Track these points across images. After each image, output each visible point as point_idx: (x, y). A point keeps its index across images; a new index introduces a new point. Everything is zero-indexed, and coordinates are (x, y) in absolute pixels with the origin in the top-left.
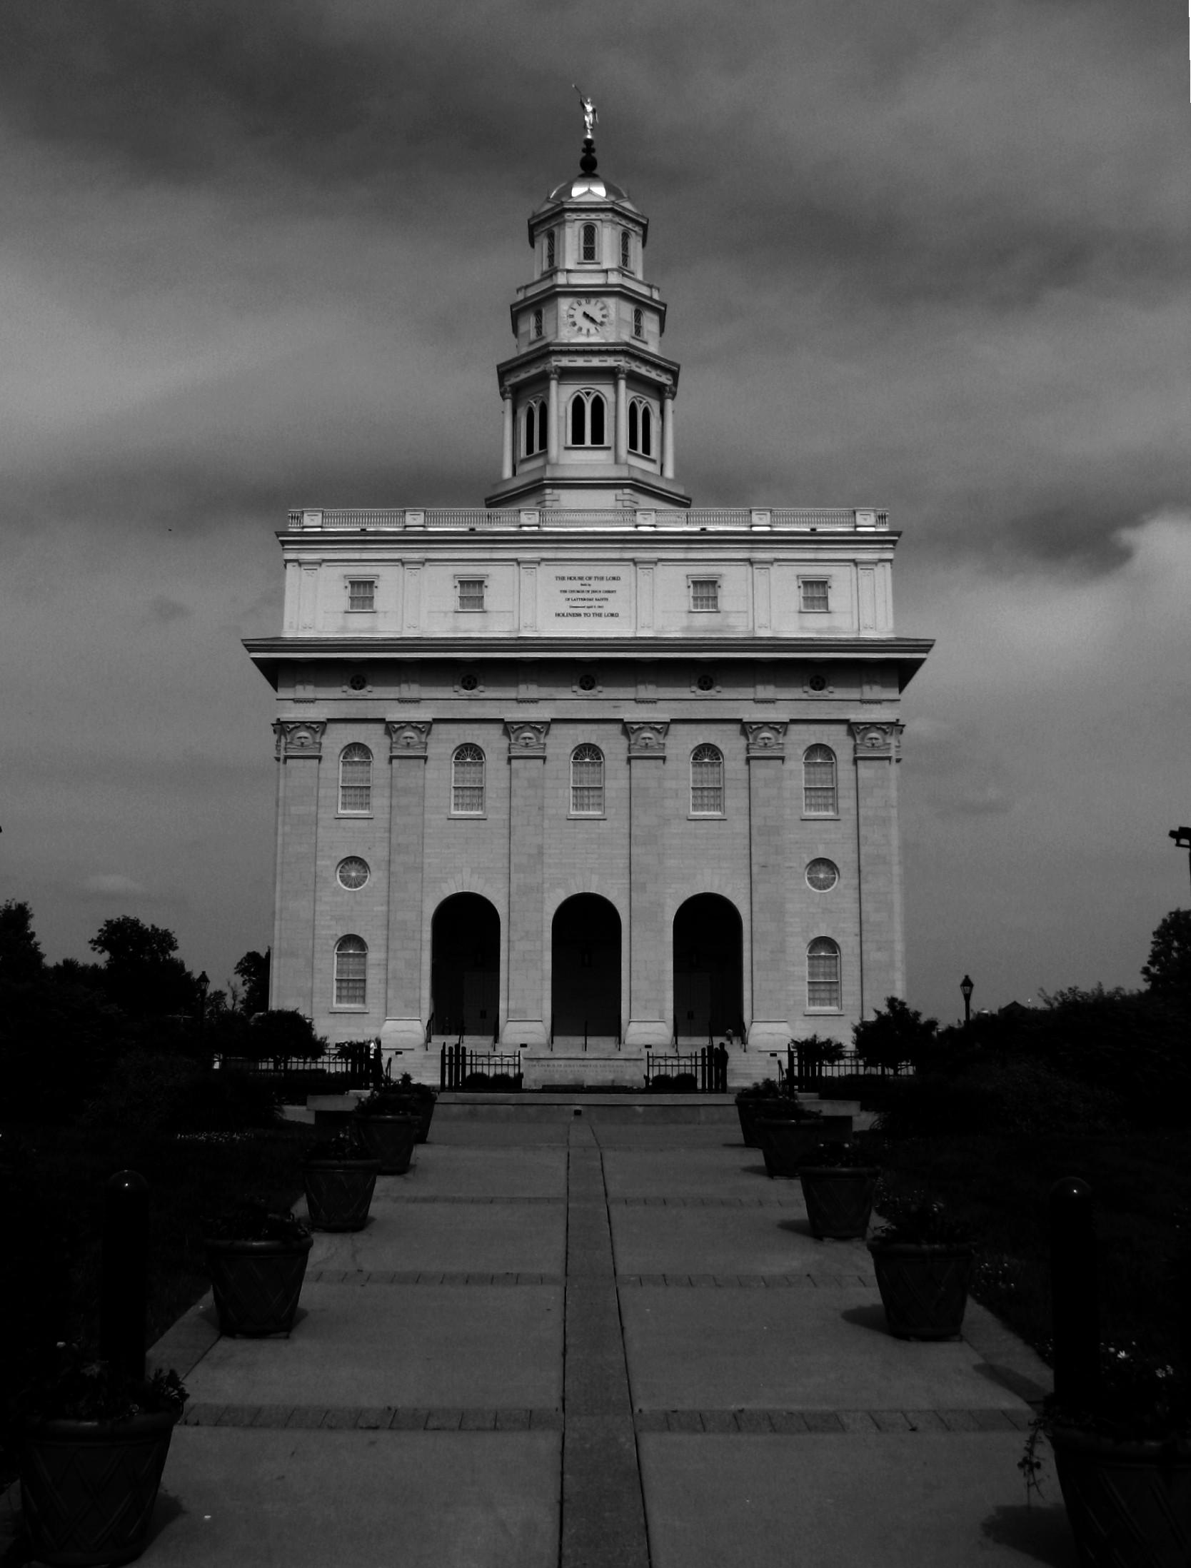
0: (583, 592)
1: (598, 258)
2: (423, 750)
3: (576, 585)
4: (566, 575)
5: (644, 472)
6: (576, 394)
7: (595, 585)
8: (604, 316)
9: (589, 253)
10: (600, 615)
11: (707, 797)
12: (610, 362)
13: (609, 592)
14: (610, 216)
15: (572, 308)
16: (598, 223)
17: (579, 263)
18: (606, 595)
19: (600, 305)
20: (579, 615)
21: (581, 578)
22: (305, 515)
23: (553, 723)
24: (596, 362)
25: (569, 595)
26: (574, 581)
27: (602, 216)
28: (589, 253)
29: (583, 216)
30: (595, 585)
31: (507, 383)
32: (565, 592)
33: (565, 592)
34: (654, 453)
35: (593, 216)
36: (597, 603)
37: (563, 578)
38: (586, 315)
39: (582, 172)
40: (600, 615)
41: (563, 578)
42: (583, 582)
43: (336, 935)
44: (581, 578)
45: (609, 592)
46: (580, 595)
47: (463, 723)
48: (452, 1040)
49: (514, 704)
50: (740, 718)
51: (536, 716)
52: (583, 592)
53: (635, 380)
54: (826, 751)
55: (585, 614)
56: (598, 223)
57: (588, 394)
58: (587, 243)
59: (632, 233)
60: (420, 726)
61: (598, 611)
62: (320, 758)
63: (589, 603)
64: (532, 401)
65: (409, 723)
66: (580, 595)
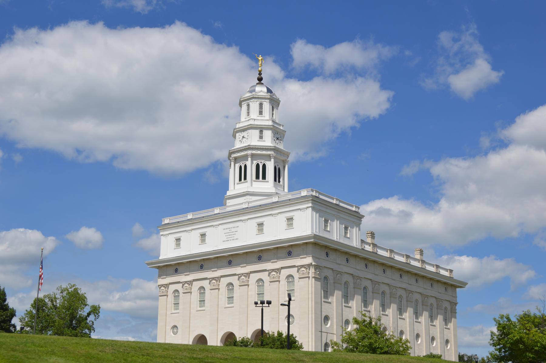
2: (247, 282)
3: (228, 231)
6: (257, 163)
7: (233, 230)
10: (233, 240)
12: (269, 153)
13: (236, 232)
15: (261, 132)
16: (249, 103)
18: (236, 233)
20: (228, 240)
21: (229, 228)
22: (302, 192)
23: (251, 273)
24: (264, 152)
25: (226, 234)
26: (227, 230)
28: (261, 113)
30: (233, 230)
31: (232, 156)
32: (225, 233)
33: (225, 233)
34: (281, 183)
36: (233, 236)
40: (233, 240)
42: (230, 229)
44: (229, 228)
45: (236, 232)
47: (257, 273)
48: (504, 318)
50: (295, 265)
51: (239, 272)
53: (253, 156)
57: (261, 162)
60: (306, 266)
62: (248, 285)
63: (231, 236)
64: (241, 163)
65: (242, 274)
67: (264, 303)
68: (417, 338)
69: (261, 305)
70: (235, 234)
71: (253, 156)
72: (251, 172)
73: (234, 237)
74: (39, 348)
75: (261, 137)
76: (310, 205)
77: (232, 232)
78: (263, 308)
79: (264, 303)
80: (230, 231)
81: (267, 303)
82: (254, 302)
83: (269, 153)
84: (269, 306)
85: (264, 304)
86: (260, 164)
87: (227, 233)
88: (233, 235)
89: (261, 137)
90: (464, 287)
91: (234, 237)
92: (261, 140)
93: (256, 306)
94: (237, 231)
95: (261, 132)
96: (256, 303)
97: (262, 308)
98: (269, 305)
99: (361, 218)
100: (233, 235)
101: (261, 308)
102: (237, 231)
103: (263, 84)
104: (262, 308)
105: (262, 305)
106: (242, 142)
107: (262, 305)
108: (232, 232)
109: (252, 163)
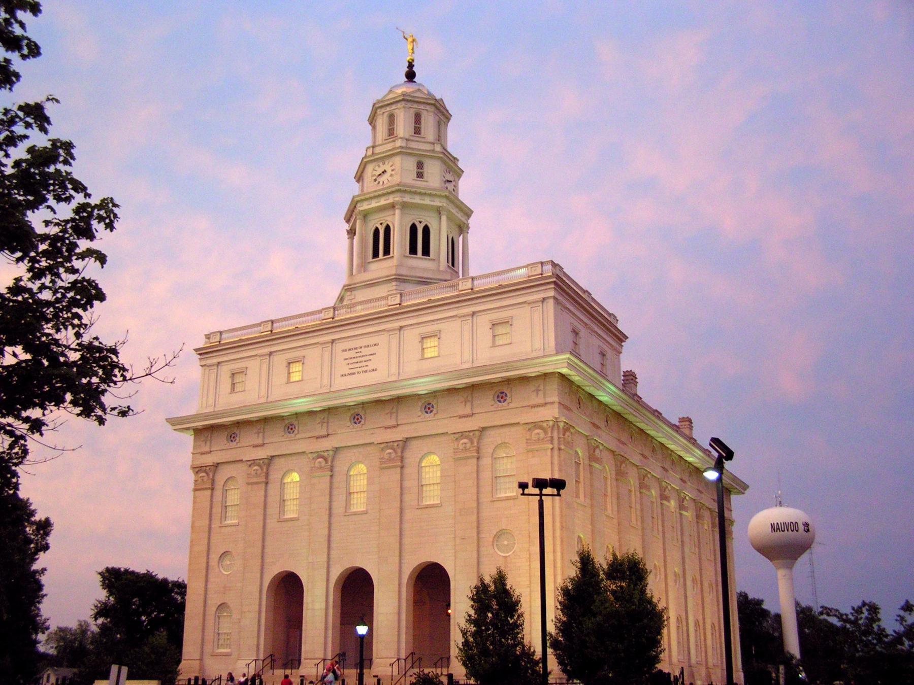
0: (357, 357)
1: (424, 133)
3: (353, 354)
4: (347, 348)
5: (425, 270)
7: (365, 351)
8: (392, 170)
9: (391, 132)
10: (366, 371)
11: (433, 490)
12: (391, 199)
13: (372, 355)
14: (403, 103)
15: (420, 165)
17: (385, 140)
18: (371, 357)
19: (391, 164)
20: (354, 374)
21: (356, 349)
27: (428, 108)
28: (391, 132)
29: (415, 106)
30: (365, 351)
35: (422, 107)
37: (346, 350)
38: (384, 172)
39: (406, 80)
40: (366, 371)
41: (346, 350)
43: (216, 604)
44: (356, 349)
45: (372, 355)
46: (355, 360)
49: (314, 440)
52: (357, 357)
53: (405, 206)
54: (630, 427)
55: (358, 372)
56: (425, 112)
58: (419, 128)
59: (396, 111)
61: (364, 369)
63: (360, 365)
66: (355, 360)
67: (527, 488)
68: (500, 587)
69: (537, 491)
70: (371, 360)
71: (405, 206)
72: (400, 240)
73: (367, 366)
74: (608, 530)
75: (420, 175)
76: (552, 293)
77: (363, 356)
78: (544, 498)
79: (527, 488)
80: (358, 355)
81: (535, 486)
82: (517, 484)
83: (391, 199)
84: (559, 495)
85: (544, 490)
86: (380, 227)
87: (351, 358)
88: (365, 361)
89: (420, 175)
90: (743, 493)
91: (367, 366)
92: (418, 179)
93: (523, 494)
94: (374, 354)
95: (420, 165)
96: (523, 486)
97: (541, 498)
98: (558, 491)
99: (622, 341)
100: (365, 361)
101: (538, 497)
102: (374, 354)
103: (415, 82)
104: (541, 498)
105: (541, 490)
106: (379, 182)
107: (541, 490)
108: (363, 356)
109: (401, 219)
